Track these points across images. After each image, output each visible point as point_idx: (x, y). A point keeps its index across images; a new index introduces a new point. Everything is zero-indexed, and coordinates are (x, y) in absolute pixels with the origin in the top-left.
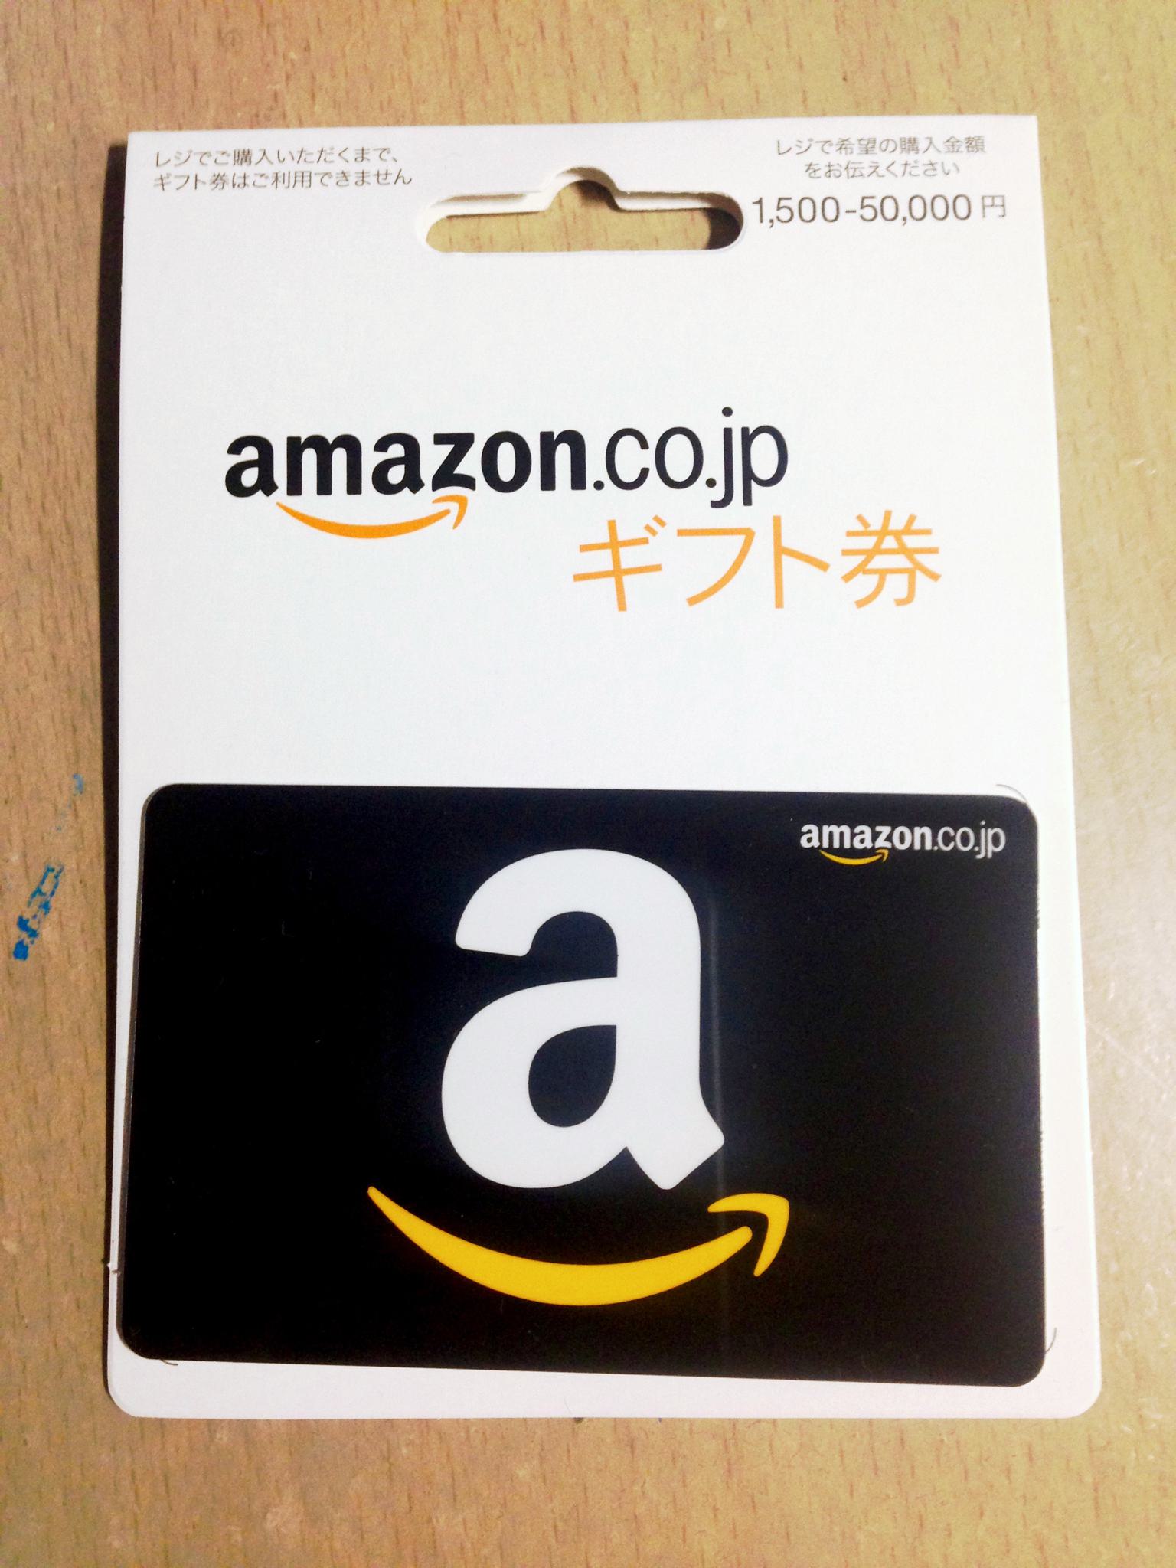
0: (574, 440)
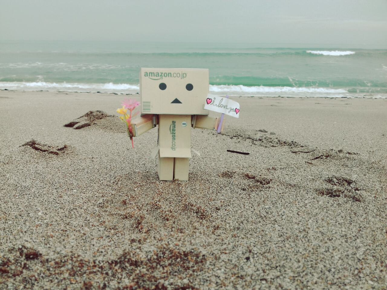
0: (171, 74)
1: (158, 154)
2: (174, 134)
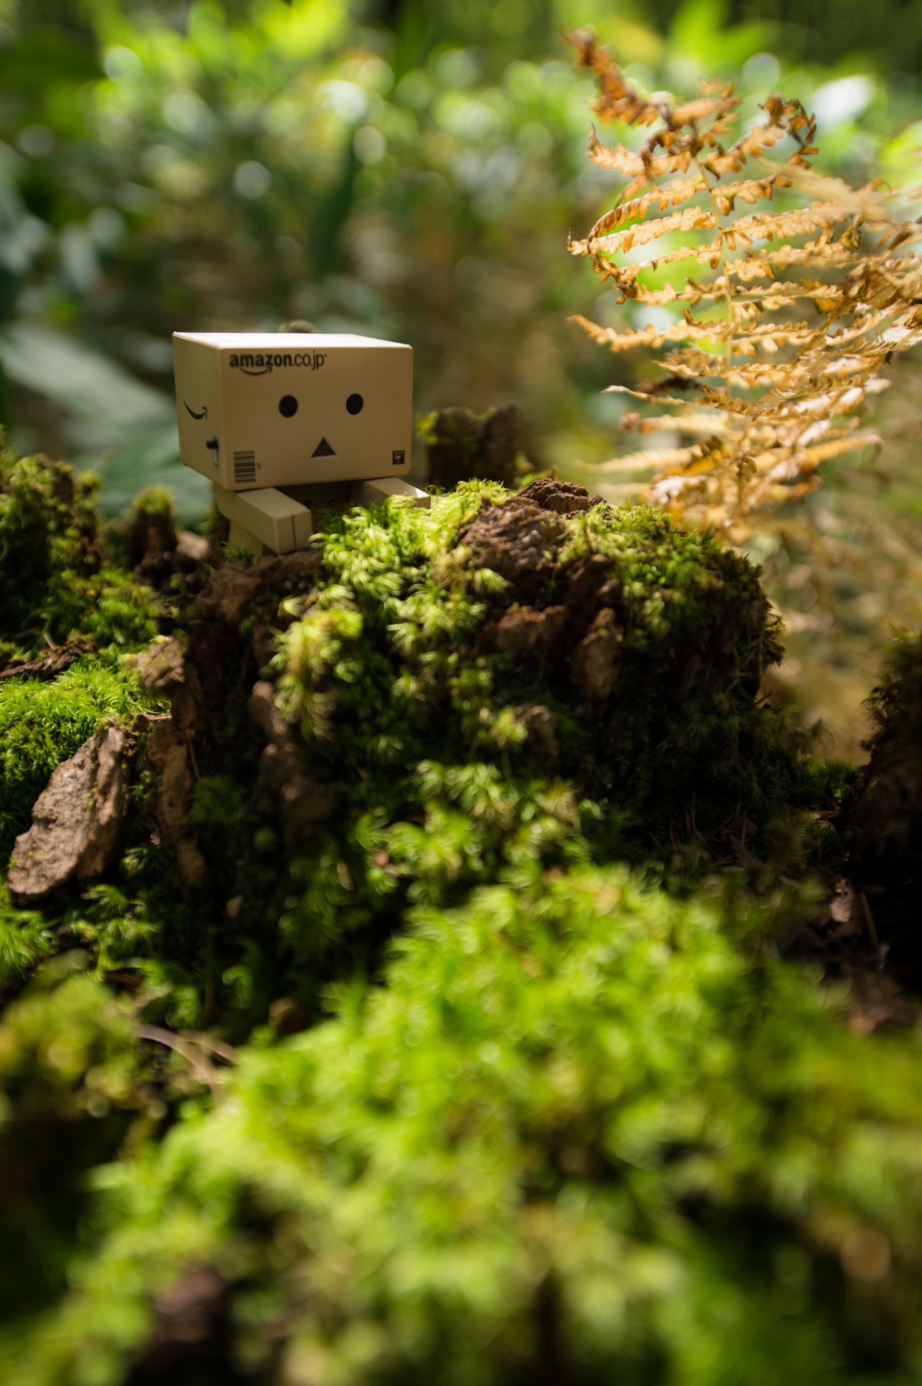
0: (290, 357)
1: (188, 773)
2: (272, 361)
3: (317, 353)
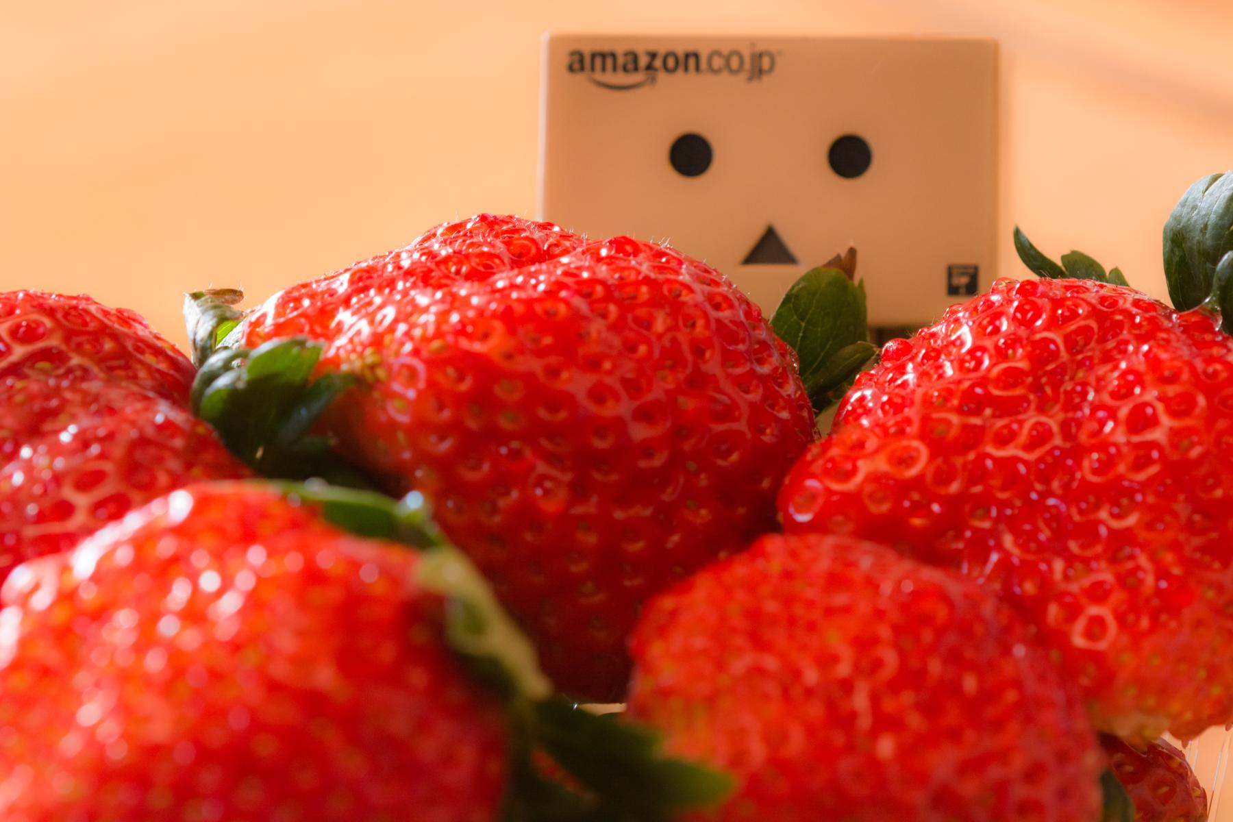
3: (760, 48)
